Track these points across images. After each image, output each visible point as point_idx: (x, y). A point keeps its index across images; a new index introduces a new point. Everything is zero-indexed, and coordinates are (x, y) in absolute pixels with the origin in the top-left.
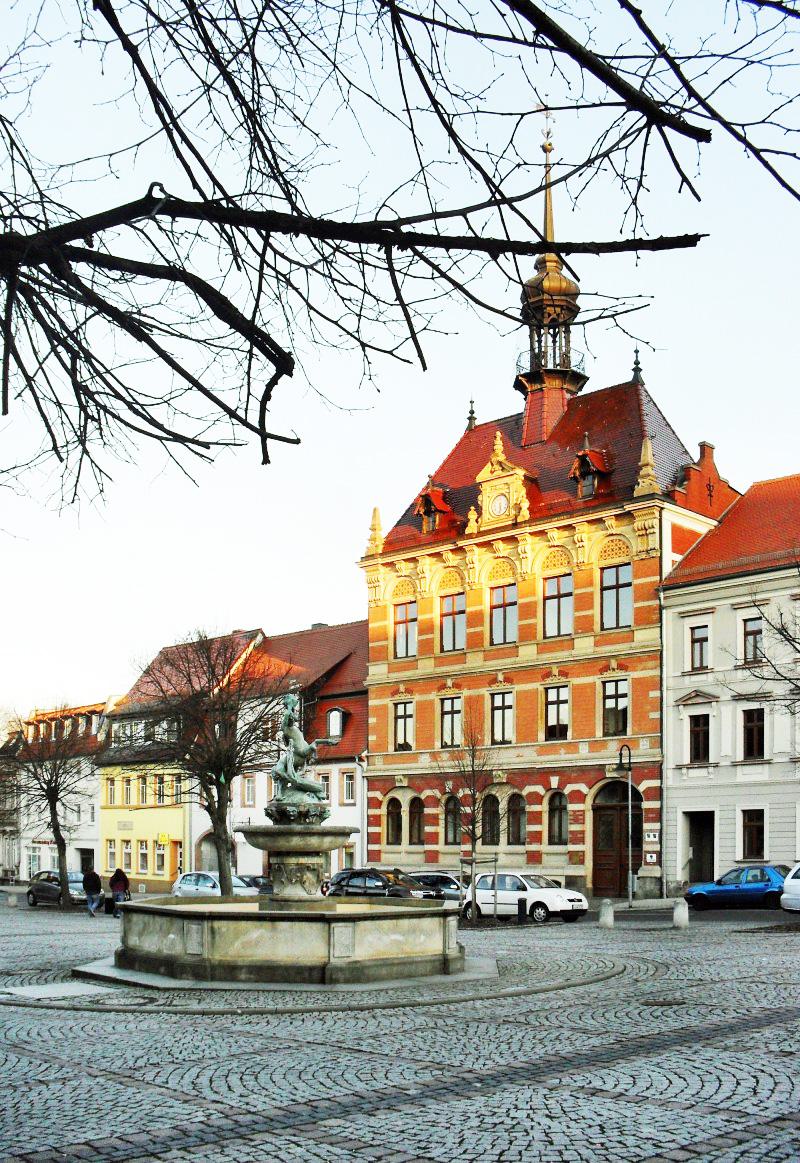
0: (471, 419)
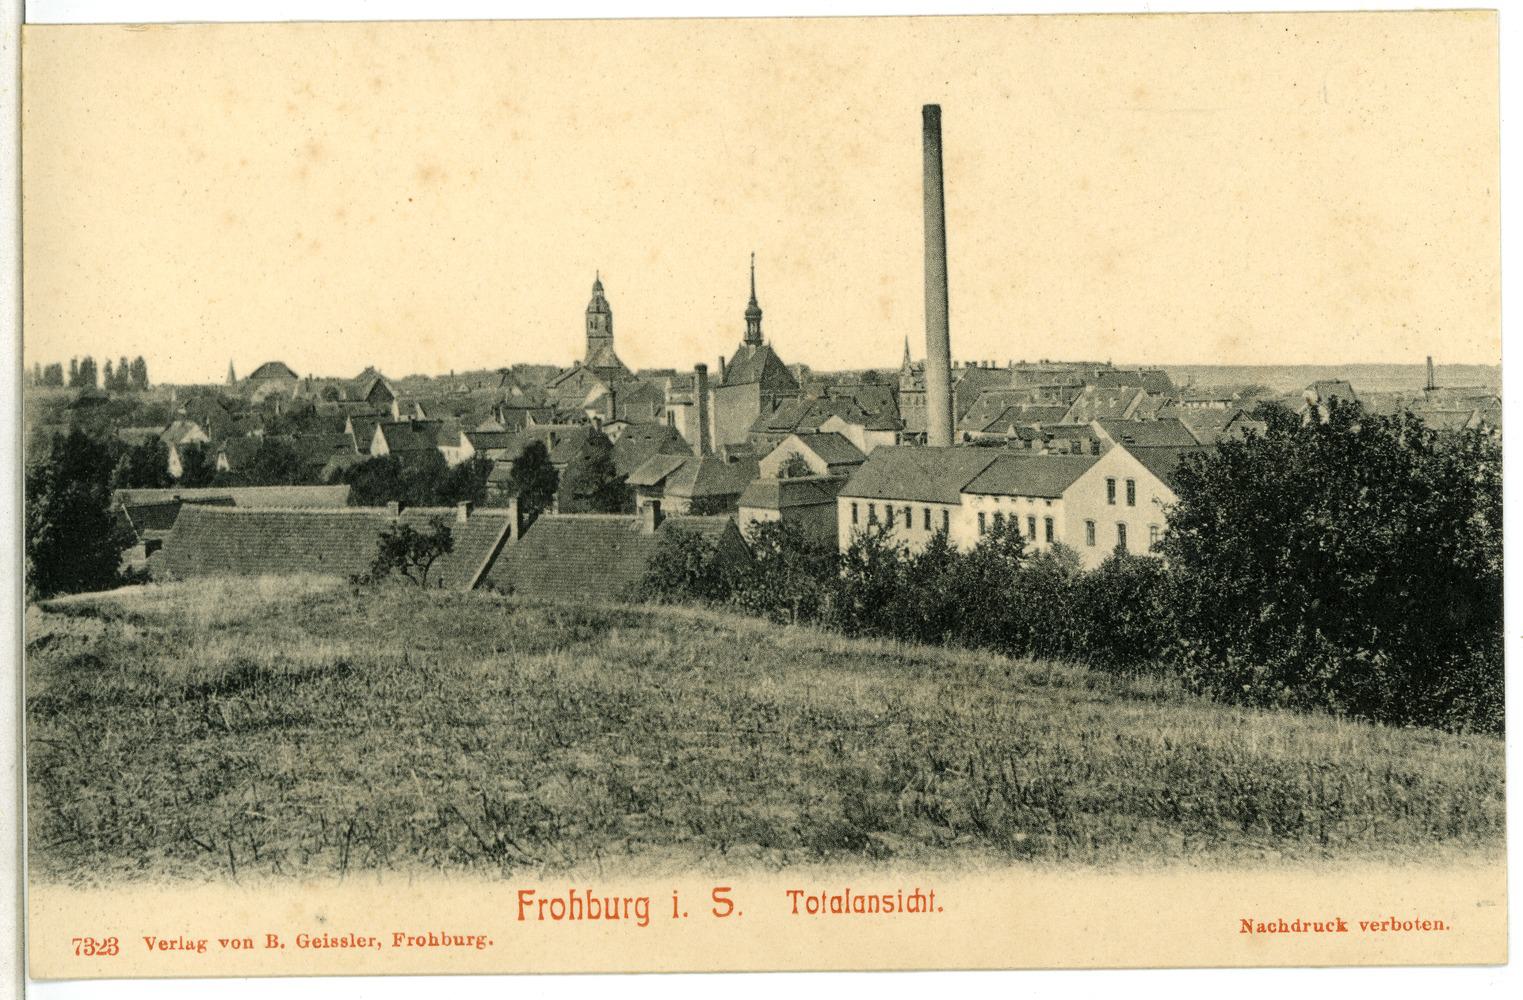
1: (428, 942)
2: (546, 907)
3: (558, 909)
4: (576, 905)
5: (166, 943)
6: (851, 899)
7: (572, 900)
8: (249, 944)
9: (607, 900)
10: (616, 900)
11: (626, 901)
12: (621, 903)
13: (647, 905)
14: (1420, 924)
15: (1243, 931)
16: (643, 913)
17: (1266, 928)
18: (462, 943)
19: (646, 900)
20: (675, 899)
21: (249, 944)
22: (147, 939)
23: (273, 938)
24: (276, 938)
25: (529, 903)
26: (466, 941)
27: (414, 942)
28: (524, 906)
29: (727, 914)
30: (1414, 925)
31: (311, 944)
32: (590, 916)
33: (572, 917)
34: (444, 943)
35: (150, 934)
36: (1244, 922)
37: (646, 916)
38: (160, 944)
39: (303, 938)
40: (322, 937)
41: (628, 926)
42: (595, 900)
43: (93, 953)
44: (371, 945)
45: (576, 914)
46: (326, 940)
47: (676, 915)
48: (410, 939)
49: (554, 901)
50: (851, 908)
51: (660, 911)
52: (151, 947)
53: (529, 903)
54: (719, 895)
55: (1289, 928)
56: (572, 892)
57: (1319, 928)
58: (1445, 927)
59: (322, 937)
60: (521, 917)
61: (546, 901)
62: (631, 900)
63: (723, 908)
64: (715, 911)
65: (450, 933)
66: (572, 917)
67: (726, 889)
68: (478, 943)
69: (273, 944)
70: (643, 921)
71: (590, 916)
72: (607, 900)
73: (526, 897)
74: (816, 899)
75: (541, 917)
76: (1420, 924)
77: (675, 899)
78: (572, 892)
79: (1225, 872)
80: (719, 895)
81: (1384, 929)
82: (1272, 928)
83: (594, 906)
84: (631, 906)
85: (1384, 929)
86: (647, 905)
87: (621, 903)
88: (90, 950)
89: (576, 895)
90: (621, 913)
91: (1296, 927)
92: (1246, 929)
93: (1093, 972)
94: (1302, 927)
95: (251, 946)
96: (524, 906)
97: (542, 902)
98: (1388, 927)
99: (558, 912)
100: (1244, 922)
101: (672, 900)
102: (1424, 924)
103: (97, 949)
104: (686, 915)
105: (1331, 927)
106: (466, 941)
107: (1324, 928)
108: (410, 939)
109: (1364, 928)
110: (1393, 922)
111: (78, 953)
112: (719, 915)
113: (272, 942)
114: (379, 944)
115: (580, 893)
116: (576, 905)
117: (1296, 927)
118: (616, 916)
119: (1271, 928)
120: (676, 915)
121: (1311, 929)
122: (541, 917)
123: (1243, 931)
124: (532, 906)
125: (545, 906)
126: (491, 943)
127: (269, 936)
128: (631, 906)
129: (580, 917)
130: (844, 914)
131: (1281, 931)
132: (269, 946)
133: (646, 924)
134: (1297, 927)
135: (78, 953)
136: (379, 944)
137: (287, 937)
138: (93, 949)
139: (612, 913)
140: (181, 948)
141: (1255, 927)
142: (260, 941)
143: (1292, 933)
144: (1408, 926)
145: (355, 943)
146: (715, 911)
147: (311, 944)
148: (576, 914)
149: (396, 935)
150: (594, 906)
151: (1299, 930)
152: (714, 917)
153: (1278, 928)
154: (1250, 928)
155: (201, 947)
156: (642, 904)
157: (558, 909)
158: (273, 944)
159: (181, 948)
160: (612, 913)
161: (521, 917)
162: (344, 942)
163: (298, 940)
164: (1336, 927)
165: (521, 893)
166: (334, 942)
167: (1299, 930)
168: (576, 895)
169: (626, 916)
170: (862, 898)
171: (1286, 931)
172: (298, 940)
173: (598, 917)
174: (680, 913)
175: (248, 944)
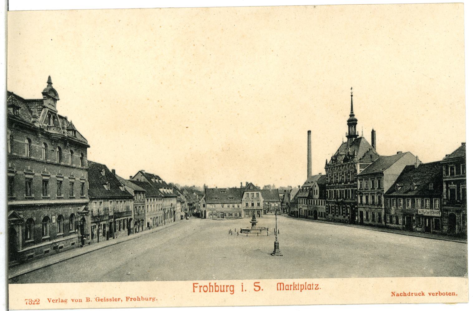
0: (343, 142)
1: (137, 300)
2: (202, 288)
3: (205, 289)
4: (211, 287)
5: (451, 293)
6: (285, 286)
7: (210, 286)
8: (81, 301)
9: (221, 286)
10: (224, 286)
11: (227, 286)
12: (225, 287)
13: (233, 288)
14: (448, 294)
15: (392, 296)
16: (232, 290)
17: (399, 294)
18: (417, 295)
19: (233, 286)
20: (242, 285)
21: (81, 301)
22: (48, 299)
23: (88, 299)
24: (89, 298)
25: (197, 287)
26: (149, 299)
27: (132, 300)
28: (195, 288)
29: (258, 291)
30: (79, 301)
31: (100, 300)
32: (216, 291)
33: (210, 291)
34: (142, 300)
35: (49, 298)
36: (392, 293)
37: (233, 291)
38: (53, 301)
39: (97, 299)
40: (103, 298)
41: (227, 294)
42: (217, 286)
43: (31, 304)
44: (150, 300)
45: (211, 290)
46: (105, 299)
47: (242, 291)
48: (131, 299)
49: (204, 286)
50: (307, 288)
51: (238, 289)
52: (50, 302)
53: (197, 287)
54: (256, 284)
55: (407, 295)
56: (210, 283)
57: (416, 295)
58: (456, 294)
59: (103, 298)
60: (194, 291)
61: (228, 286)
62: (202, 286)
63: (257, 288)
64: (255, 289)
65: (144, 297)
66: (210, 291)
67: (259, 283)
68: (153, 300)
69: (88, 300)
70: (232, 292)
71: (216, 291)
72: (221, 286)
73: (196, 285)
74: (206, 286)
75: (200, 291)
76: (448, 294)
77: (242, 285)
78: (210, 283)
79: (353, 278)
80: (256, 284)
81: (436, 295)
82: (401, 295)
83: (217, 288)
84: (228, 288)
85: (56, 302)
86: (233, 288)
87: (225, 287)
88: (30, 303)
89: (211, 285)
90: (225, 290)
91: (409, 294)
92: (393, 295)
93: (194, 308)
94: (411, 294)
95: (81, 301)
96: (195, 288)
97: (200, 287)
98: (438, 295)
99: (205, 290)
100: (392, 293)
101: (241, 286)
102: (449, 294)
103: (33, 302)
104: (246, 291)
105: (420, 294)
106: (149, 299)
107: (418, 295)
108: (131, 299)
109: (430, 295)
110: (440, 293)
111: (27, 304)
112: (256, 291)
113: (88, 300)
114: (122, 300)
115: (213, 284)
116: (211, 287)
117: (409, 294)
118: (224, 291)
119: (401, 295)
120: (242, 291)
121: (414, 295)
122: (200, 291)
123: (392, 296)
124: (198, 288)
125: (228, 287)
126: (157, 300)
127: (87, 298)
128: (228, 288)
129: (213, 291)
130: (312, 290)
131: (404, 296)
132: (87, 301)
133: (233, 293)
134: (409, 294)
135: (27, 304)
136: (122, 300)
137: (92, 298)
138: (32, 303)
139: (222, 290)
140: (59, 302)
141: (396, 294)
142: (84, 300)
143: (407, 296)
144: (444, 294)
145: (114, 300)
146: (255, 289)
147: (100, 300)
148: (211, 290)
149: (127, 297)
150: (217, 288)
151: (410, 295)
152: (254, 290)
153: (403, 294)
154: (394, 295)
155: (127, 298)
156: (232, 287)
157: (205, 289)
158: (88, 300)
159: (59, 302)
160: (222, 290)
161: (194, 291)
162: (111, 300)
163: (96, 299)
164: (421, 294)
165: (194, 284)
166: (107, 300)
167: (410, 295)
168: (211, 285)
169: (227, 291)
170: (288, 285)
171: (406, 295)
172: (96, 299)
173: (218, 291)
174: (244, 290)
175: (80, 300)
